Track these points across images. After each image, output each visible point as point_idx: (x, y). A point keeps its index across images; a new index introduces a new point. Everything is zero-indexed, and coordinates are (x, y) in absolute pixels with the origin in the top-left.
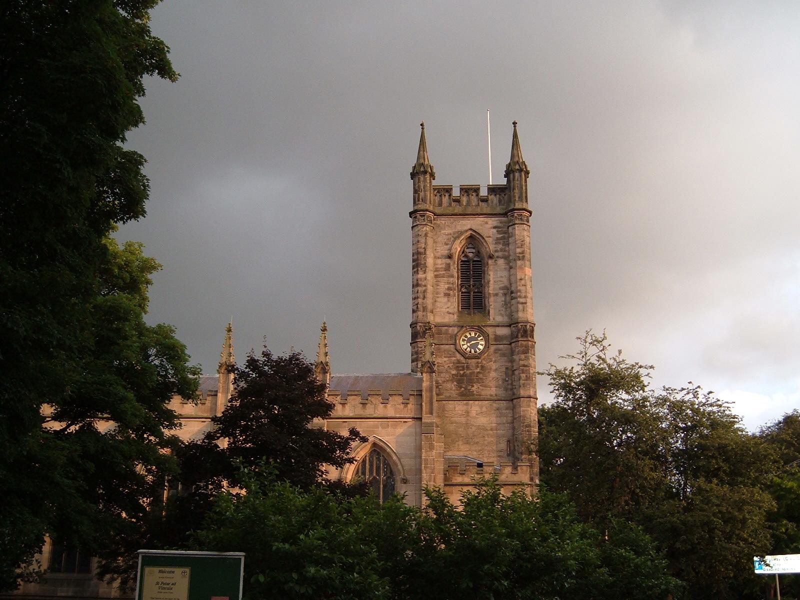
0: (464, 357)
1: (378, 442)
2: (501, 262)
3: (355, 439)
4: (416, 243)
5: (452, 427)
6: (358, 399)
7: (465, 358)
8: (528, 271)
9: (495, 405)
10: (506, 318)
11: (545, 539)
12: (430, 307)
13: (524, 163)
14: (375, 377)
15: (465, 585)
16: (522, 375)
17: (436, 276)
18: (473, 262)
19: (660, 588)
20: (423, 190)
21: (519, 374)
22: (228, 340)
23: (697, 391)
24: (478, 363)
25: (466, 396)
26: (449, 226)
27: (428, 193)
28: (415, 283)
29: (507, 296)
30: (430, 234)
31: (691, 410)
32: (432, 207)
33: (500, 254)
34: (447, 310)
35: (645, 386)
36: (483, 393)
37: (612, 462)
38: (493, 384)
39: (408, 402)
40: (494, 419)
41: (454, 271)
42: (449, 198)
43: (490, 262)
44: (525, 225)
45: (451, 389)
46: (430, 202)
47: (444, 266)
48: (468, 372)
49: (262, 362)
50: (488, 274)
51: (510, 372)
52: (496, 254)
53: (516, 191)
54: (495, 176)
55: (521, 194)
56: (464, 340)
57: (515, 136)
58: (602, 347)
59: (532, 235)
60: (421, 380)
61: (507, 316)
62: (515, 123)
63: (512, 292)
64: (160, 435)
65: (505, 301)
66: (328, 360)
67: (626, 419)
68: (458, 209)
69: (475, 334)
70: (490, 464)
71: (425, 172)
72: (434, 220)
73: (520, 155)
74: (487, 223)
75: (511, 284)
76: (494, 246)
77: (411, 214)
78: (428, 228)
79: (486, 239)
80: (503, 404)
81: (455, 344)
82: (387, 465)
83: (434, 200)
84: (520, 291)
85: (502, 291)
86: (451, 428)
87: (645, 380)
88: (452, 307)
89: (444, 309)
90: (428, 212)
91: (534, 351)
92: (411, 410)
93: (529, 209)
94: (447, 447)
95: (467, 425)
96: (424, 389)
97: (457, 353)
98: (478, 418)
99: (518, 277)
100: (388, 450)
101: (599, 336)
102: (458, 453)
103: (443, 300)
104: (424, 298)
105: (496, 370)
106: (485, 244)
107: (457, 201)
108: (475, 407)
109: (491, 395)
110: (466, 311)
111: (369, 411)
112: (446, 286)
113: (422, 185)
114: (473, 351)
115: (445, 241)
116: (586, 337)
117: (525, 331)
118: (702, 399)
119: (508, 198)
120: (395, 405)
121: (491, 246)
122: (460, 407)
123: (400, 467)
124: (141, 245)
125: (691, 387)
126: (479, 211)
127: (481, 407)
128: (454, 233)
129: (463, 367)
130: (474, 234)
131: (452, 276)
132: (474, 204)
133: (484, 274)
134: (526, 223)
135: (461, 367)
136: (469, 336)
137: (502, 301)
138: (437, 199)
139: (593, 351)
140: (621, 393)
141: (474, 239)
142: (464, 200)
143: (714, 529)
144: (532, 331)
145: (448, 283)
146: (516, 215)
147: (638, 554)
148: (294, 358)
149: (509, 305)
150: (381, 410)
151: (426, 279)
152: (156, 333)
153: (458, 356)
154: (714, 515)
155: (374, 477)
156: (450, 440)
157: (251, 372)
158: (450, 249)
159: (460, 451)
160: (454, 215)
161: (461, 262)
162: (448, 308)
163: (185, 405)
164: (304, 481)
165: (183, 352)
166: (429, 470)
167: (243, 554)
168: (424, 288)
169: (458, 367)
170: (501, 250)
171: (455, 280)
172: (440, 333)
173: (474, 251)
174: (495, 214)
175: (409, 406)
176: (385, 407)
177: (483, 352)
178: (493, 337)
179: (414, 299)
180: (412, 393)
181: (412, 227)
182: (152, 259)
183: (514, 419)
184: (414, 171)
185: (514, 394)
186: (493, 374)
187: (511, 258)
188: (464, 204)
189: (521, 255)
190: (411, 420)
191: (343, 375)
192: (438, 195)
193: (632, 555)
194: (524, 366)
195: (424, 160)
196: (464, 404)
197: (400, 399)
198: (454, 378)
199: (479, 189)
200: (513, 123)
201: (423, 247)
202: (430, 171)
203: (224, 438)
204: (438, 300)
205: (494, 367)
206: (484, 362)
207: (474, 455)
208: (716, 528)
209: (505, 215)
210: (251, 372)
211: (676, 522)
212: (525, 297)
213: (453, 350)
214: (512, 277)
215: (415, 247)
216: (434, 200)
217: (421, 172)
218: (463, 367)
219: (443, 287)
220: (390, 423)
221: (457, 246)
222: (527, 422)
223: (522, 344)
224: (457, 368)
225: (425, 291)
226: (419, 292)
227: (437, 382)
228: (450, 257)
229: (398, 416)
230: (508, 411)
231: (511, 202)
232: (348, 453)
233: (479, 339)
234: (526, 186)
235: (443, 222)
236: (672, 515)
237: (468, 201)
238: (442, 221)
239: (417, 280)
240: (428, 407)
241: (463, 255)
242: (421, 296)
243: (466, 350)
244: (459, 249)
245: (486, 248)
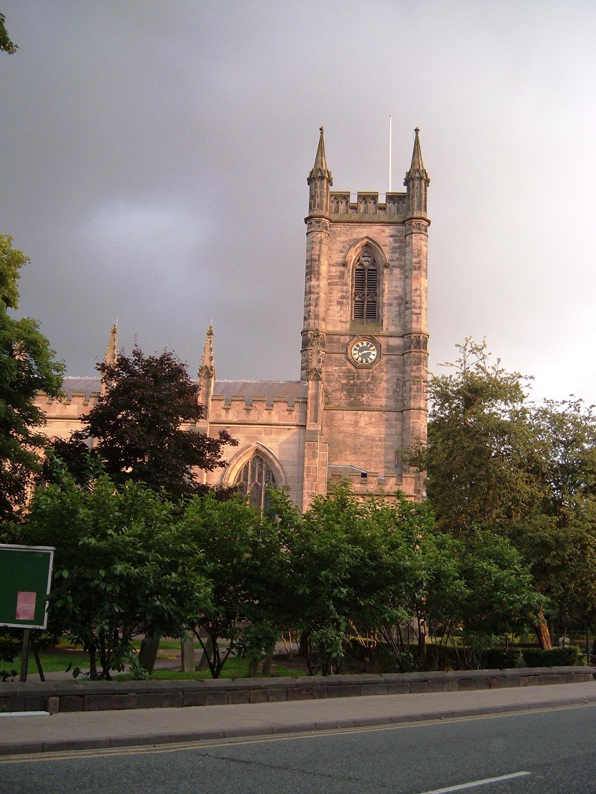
0: (355, 367)
1: (261, 448)
2: (397, 271)
3: (225, 442)
4: (310, 250)
5: (340, 437)
6: (243, 405)
8: (424, 281)
9: (384, 416)
10: (400, 328)
11: (394, 546)
12: (322, 315)
13: (424, 171)
14: (264, 384)
15: (301, 591)
16: (413, 387)
17: (330, 284)
18: (368, 270)
19: (521, 603)
20: (319, 196)
21: (410, 385)
22: (113, 342)
23: (578, 405)
25: (356, 406)
27: (325, 199)
28: (308, 291)
29: (402, 306)
31: (573, 424)
32: (328, 213)
33: (396, 263)
34: (340, 318)
35: (525, 397)
36: (373, 403)
37: (484, 473)
38: (383, 394)
39: (292, 409)
40: (383, 430)
41: (349, 279)
42: (346, 205)
43: (386, 271)
45: (340, 399)
46: (327, 208)
47: (338, 274)
49: (132, 362)
50: (382, 283)
51: (401, 384)
52: (392, 264)
53: (415, 199)
54: (393, 183)
55: (420, 203)
56: (355, 350)
58: (482, 355)
59: (437, 244)
60: (307, 388)
61: (400, 325)
62: (417, 130)
63: (407, 303)
64: (26, 433)
65: (399, 311)
66: (213, 364)
67: (502, 430)
68: (355, 217)
69: (368, 344)
70: (375, 475)
71: (322, 178)
72: (330, 227)
73: (421, 163)
74: (383, 231)
75: (406, 294)
76: (390, 255)
77: (306, 220)
79: (383, 248)
80: (393, 415)
81: (346, 353)
82: (269, 472)
83: (331, 207)
84: (414, 301)
85: (396, 302)
86: (339, 437)
87: (525, 391)
88: (345, 316)
89: (337, 317)
90: (323, 219)
91: (427, 362)
92: (295, 416)
93: (428, 218)
94: (332, 456)
95: (356, 435)
96: (309, 396)
97: (348, 362)
98: (366, 428)
99: (414, 288)
100: (271, 457)
101: (480, 344)
102: (345, 462)
104: (316, 305)
105: (387, 381)
106: (381, 253)
107: (355, 208)
108: (364, 418)
109: (381, 406)
110: (359, 320)
111: (253, 417)
112: (340, 294)
113: (318, 190)
114: (364, 361)
115: (339, 250)
116: (466, 345)
117: (418, 342)
118: (583, 412)
119: (406, 208)
120: (280, 412)
122: (349, 417)
123: (282, 474)
124: (10, 239)
125: (573, 399)
126: (376, 219)
127: (370, 417)
128: (350, 241)
129: (354, 376)
131: (346, 284)
132: (371, 212)
133: (379, 283)
134: (424, 233)
138: (334, 205)
139: (472, 359)
140: (499, 403)
141: (370, 247)
142: (362, 207)
143: (586, 545)
144: (426, 342)
145: (342, 291)
146: (413, 224)
147: (502, 567)
148: (165, 360)
149: (403, 316)
150: (265, 417)
151: (319, 286)
152: (18, 327)
153: (349, 366)
154: (588, 531)
155: (256, 484)
156: (335, 448)
157: (121, 372)
158: (345, 257)
159: (348, 461)
160: (351, 223)
161: (356, 270)
162: (341, 316)
163: (67, 406)
164: (168, 482)
165: (44, 347)
166: (311, 478)
167: (53, 548)
168: (317, 296)
169: (349, 376)
170: (397, 259)
171: (350, 289)
172: (331, 341)
173: (370, 259)
174: (394, 223)
175: (294, 413)
176: (269, 413)
177: (374, 362)
179: (306, 306)
180: (298, 400)
181: (307, 234)
182: (19, 252)
183: (403, 430)
184: (310, 177)
185: (404, 405)
186: (384, 385)
187: (407, 268)
188: (362, 211)
189: (417, 265)
190: (295, 427)
191: (231, 381)
192: (335, 201)
193: (494, 568)
194: (416, 377)
195: (322, 165)
197: (284, 406)
198: (343, 387)
199: (377, 196)
200: (415, 130)
201: (317, 254)
202: (327, 176)
203: (93, 437)
204: (331, 308)
205: (385, 378)
207: (361, 465)
208: (590, 545)
209: (403, 223)
210: (121, 372)
211: (546, 537)
212: (420, 308)
214: (407, 288)
215: (309, 253)
216: (331, 207)
217: (318, 177)
218: (354, 376)
219: (336, 295)
220: (273, 430)
221: (353, 255)
222: (416, 434)
223: (414, 355)
224: (347, 378)
225: (317, 299)
226: (312, 299)
227: (326, 391)
228: (344, 265)
229: (282, 422)
230: (397, 423)
231: (409, 210)
232: (220, 457)
233: (371, 349)
234: (426, 195)
235: (339, 229)
236: (544, 528)
237: (365, 208)
238: (338, 228)
239: (310, 288)
240: (313, 414)
241: (358, 263)
242: (314, 304)
243: (357, 359)
244: (354, 257)
245: (382, 257)
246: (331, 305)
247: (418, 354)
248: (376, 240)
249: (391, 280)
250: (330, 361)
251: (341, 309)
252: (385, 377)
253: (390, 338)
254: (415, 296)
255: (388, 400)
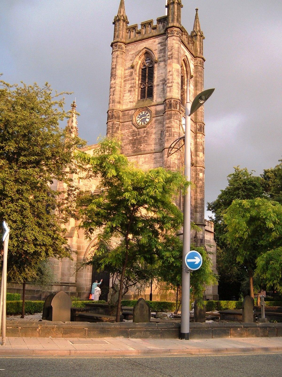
7: (138, 129)
12: (117, 100)
17: (125, 81)
24: (145, 130)
25: (137, 152)
26: (133, 49)
30: (120, 56)
34: (130, 100)
36: (147, 149)
44: (174, 37)
45: (128, 149)
47: (129, 74)
48: (139, 137)
52: (160, 60)
56: (138, 117)
57: (197, 14)
62: (197, 10)
68: (139, 37)
69: (145, 113)
76: (158, 55)
78: (118, 53)
80: (158, 155)
84: (168, 79)
85: (161, 82)
88: (132, 98)
98: (142, 165)
103: (128, 94)
105: (155, 133)
108: (142, 159)
109: (151, 150)
114: (143, 124)
115: (132, 58)
117: (170, 105)
121: (156, 56)
127: (145, 158)
128: (136, 53)
130: (147, 50)
135: (135, 134)
136: (141, 114)
137: (161, 89)
141: (148, 54)
142: (144, 31)
151: (115, 83)
153: (134, 128)
168: (114, 89)
169: (133, 135)
170: (163, 56)
177: (148, 123)
178: (154, 112)
186: (153, 136)
188: (144, 33)
194: (168, 127)
196: (136, 158)
204: (125, 95)
205: (154, 132)
206: (148, 129)
213: (131, 124)
218: (136, 134)
224: (133, 136)
230: (160, 159)
233: (147, 115)
235: (130, 47)
243: (139, 123)
246: (125, 94)
247: (170, 112)
248: (151, 48)
249: (159, 70)
250: (123, 127)
251: (130, 94)
252: (154, 131)
253: (157, 106)
254: (169, 75)
255: (155, 145)
